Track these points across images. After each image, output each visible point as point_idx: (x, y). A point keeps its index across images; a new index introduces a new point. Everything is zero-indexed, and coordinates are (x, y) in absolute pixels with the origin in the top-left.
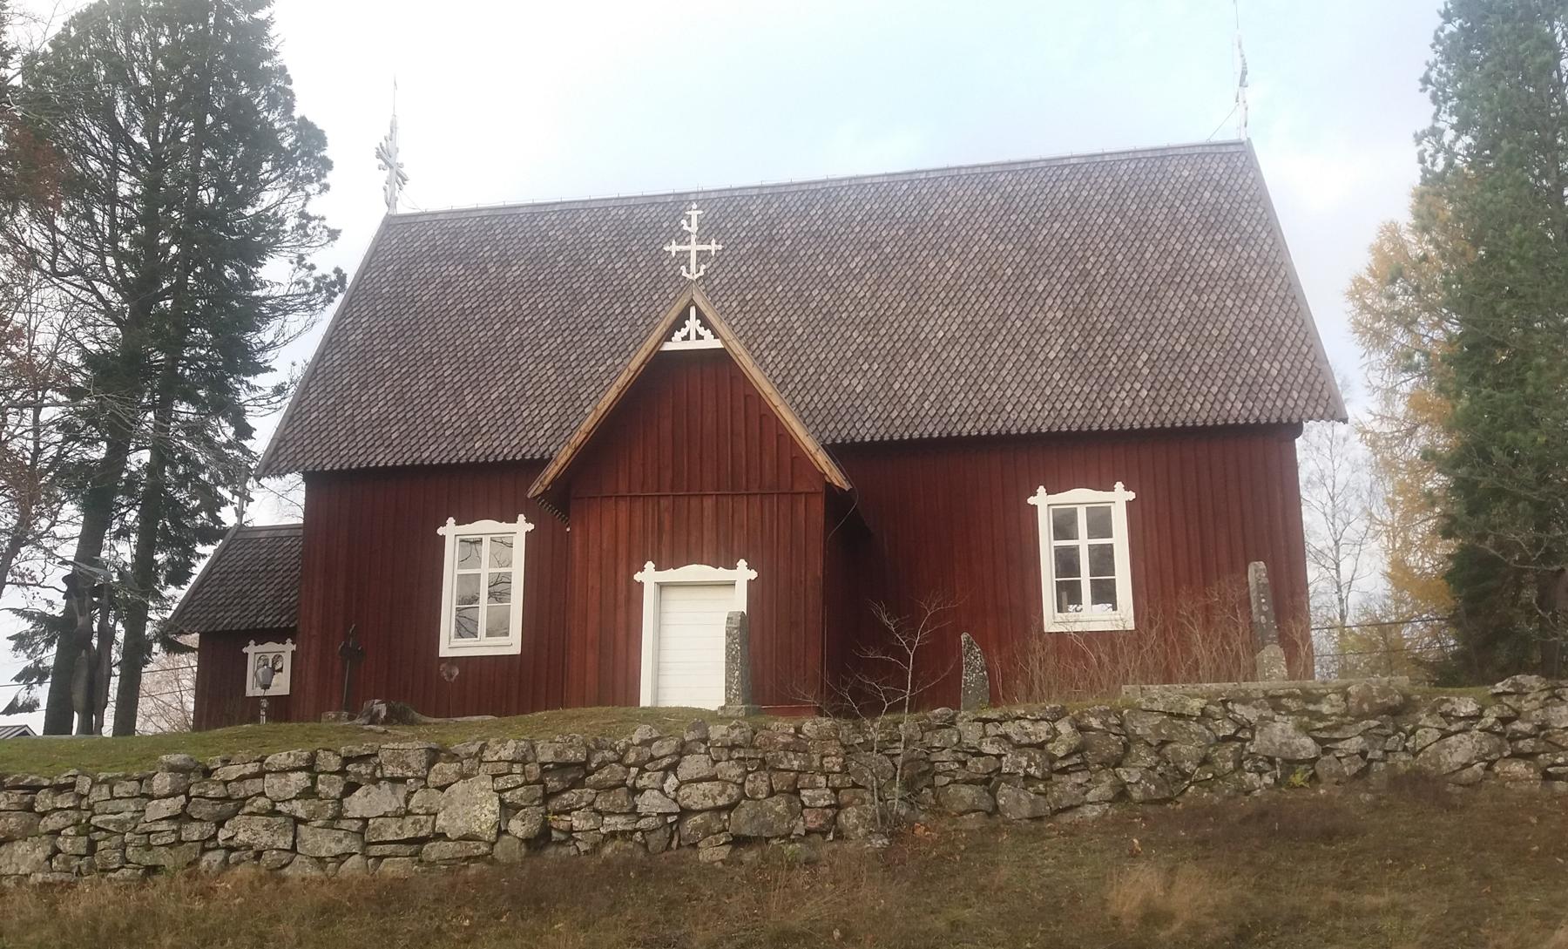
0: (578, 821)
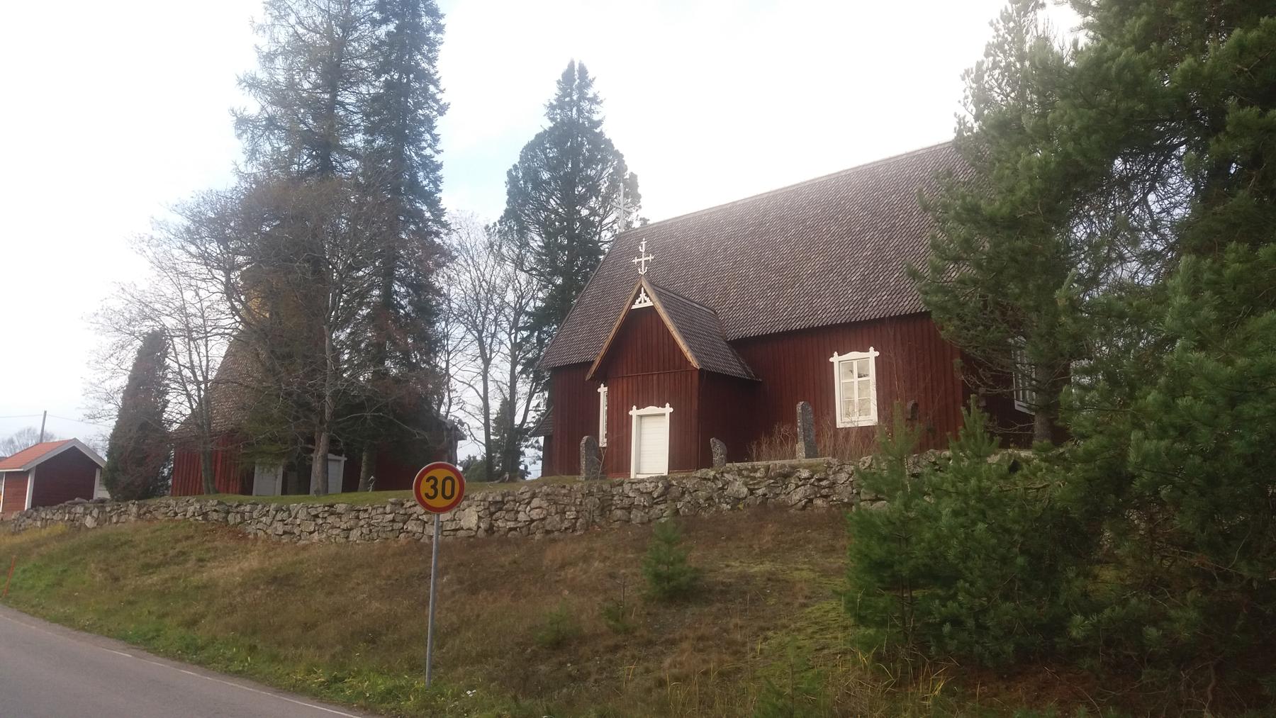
0: (500, 523)
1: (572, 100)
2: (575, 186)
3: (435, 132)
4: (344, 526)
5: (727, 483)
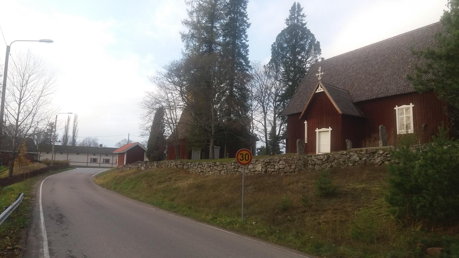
0: (269, 169)
1: (295, 17)
2: (296, 48)
3: (246, 34)
4: (219, 170)
5: (351, 156)
